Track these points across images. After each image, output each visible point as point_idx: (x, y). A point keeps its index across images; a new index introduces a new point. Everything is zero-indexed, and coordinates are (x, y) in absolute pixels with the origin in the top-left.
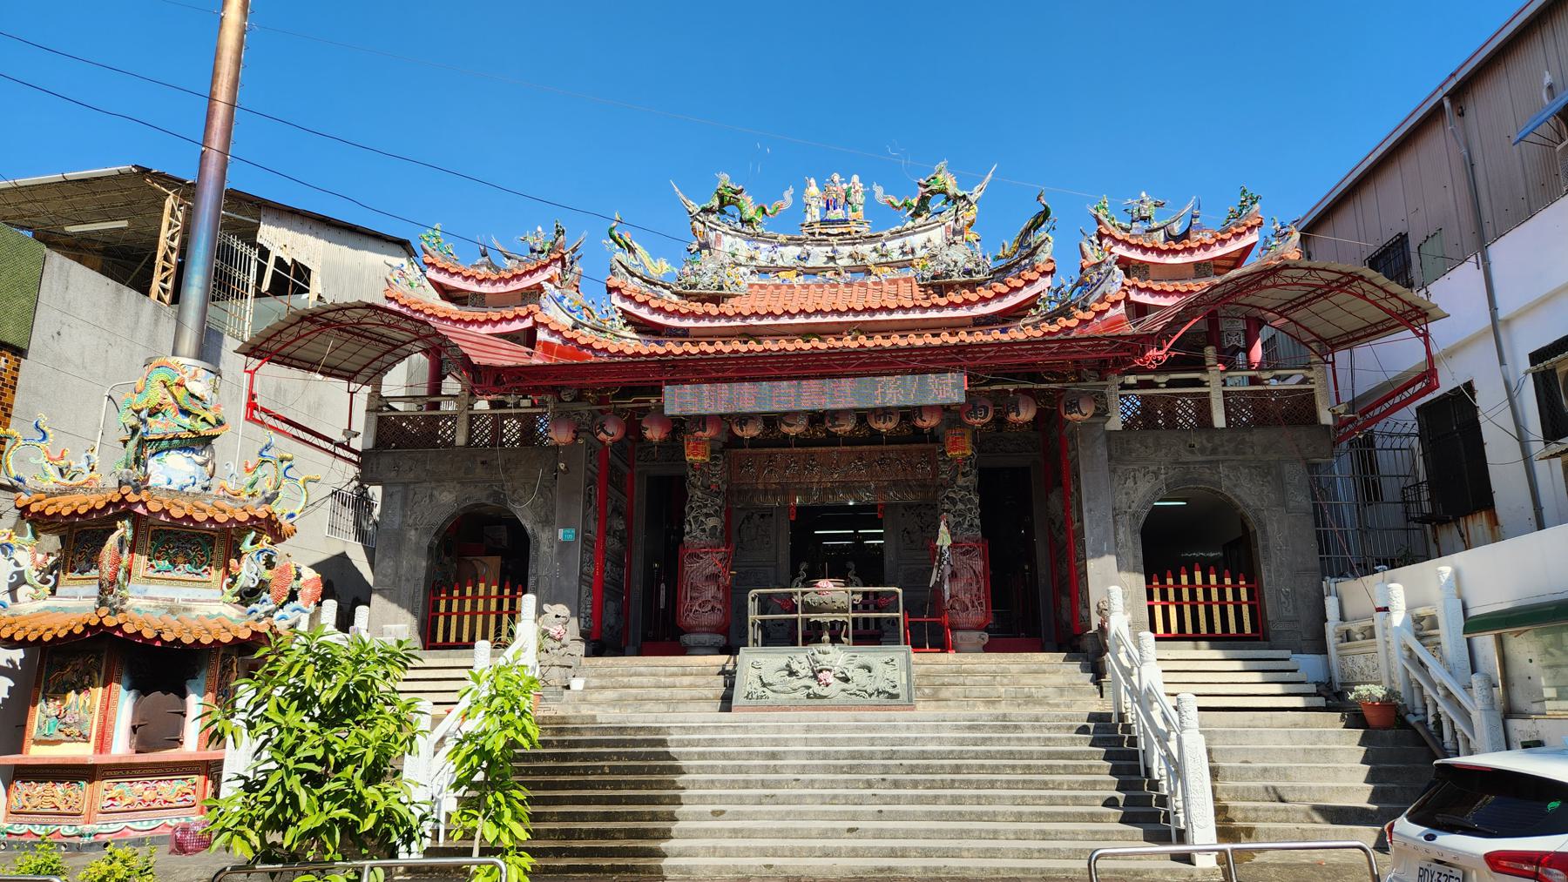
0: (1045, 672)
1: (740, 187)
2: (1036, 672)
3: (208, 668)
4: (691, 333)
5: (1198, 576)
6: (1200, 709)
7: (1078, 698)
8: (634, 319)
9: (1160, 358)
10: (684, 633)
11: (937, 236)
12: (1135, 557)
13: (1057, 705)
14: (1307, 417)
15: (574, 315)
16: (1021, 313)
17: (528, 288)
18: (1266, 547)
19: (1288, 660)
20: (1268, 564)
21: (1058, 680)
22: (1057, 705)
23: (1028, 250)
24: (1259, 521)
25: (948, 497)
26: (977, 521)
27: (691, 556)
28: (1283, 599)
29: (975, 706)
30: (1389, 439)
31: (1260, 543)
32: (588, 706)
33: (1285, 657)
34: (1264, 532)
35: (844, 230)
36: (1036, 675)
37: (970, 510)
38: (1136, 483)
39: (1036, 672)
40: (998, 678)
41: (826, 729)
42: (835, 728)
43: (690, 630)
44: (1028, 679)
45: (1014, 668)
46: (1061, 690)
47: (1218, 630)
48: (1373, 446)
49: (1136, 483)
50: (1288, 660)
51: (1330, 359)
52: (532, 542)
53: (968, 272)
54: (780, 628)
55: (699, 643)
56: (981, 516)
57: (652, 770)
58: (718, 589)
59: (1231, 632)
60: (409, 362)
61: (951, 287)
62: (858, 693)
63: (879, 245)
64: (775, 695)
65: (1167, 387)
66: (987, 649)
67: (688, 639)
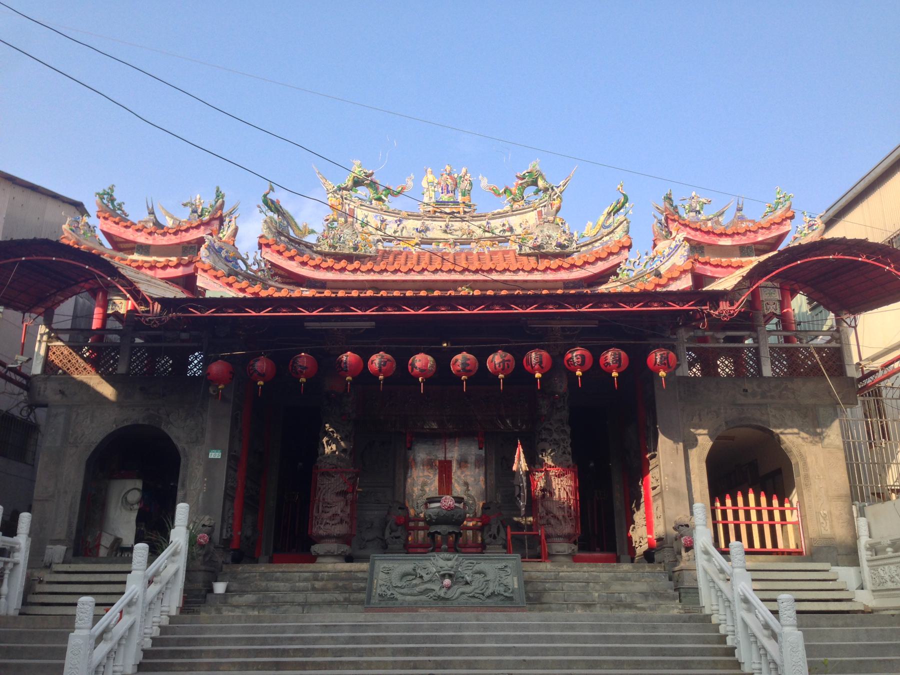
0: (629, 580)
1: (370, 172)
2: (622, 579)
3: (416, 467)
4: (328, 285)
5: (751, 497)
6: (798, 612)
7: (661, 602)
8: (280, 272)
9: (732, 312)
10: (314, 543)
11: (532, 217)
12: (702, 482)
13: (643, 609)
14: (835, 370)
15: (230, 264)
16: (602, 280)
17: (189, 242)
18: (807, 477)
19: (827, 571)
20: (809, 491)
21: (642, 587)
22: (643, 609)
23: (610, 229)
24: (801, 455)
25: (545, 429)
26: (569, 449)
27: (323, 474)
28: (822, 520)
29: (574, 609)
30: (891, 391)
31: (802, 473)
32: (230, 608)
33: (825, 569)
34: (805, 464)
35: (455, 210)
36: (623, 582)
37: (563, 440)
38: (701, 420)
39: (622, 579)
40: (591, 584)
41: (378, 628)
42: (387, 628)
43: (320, 539)
44: (616, 587)
45: (604, 576)
46: (645, 595)
47: (757, 545)
48: (881, 396)
49: (701, 420)
50: (827, 571)
51: (853, 324)
52: (182, 460)
53: (559, 245)
54: (397, 540)
55: (329, 552)
56: (571, 445)
57: (189, 654)
58: (347, 505)
59: (756, 547)
60: (76, 301)
61: (545, 256)
62: (477, 595)
63: (484, 223)
64: (403, 598)
65: (725, 342)
66: (576, 559)
67: (316, 548)
